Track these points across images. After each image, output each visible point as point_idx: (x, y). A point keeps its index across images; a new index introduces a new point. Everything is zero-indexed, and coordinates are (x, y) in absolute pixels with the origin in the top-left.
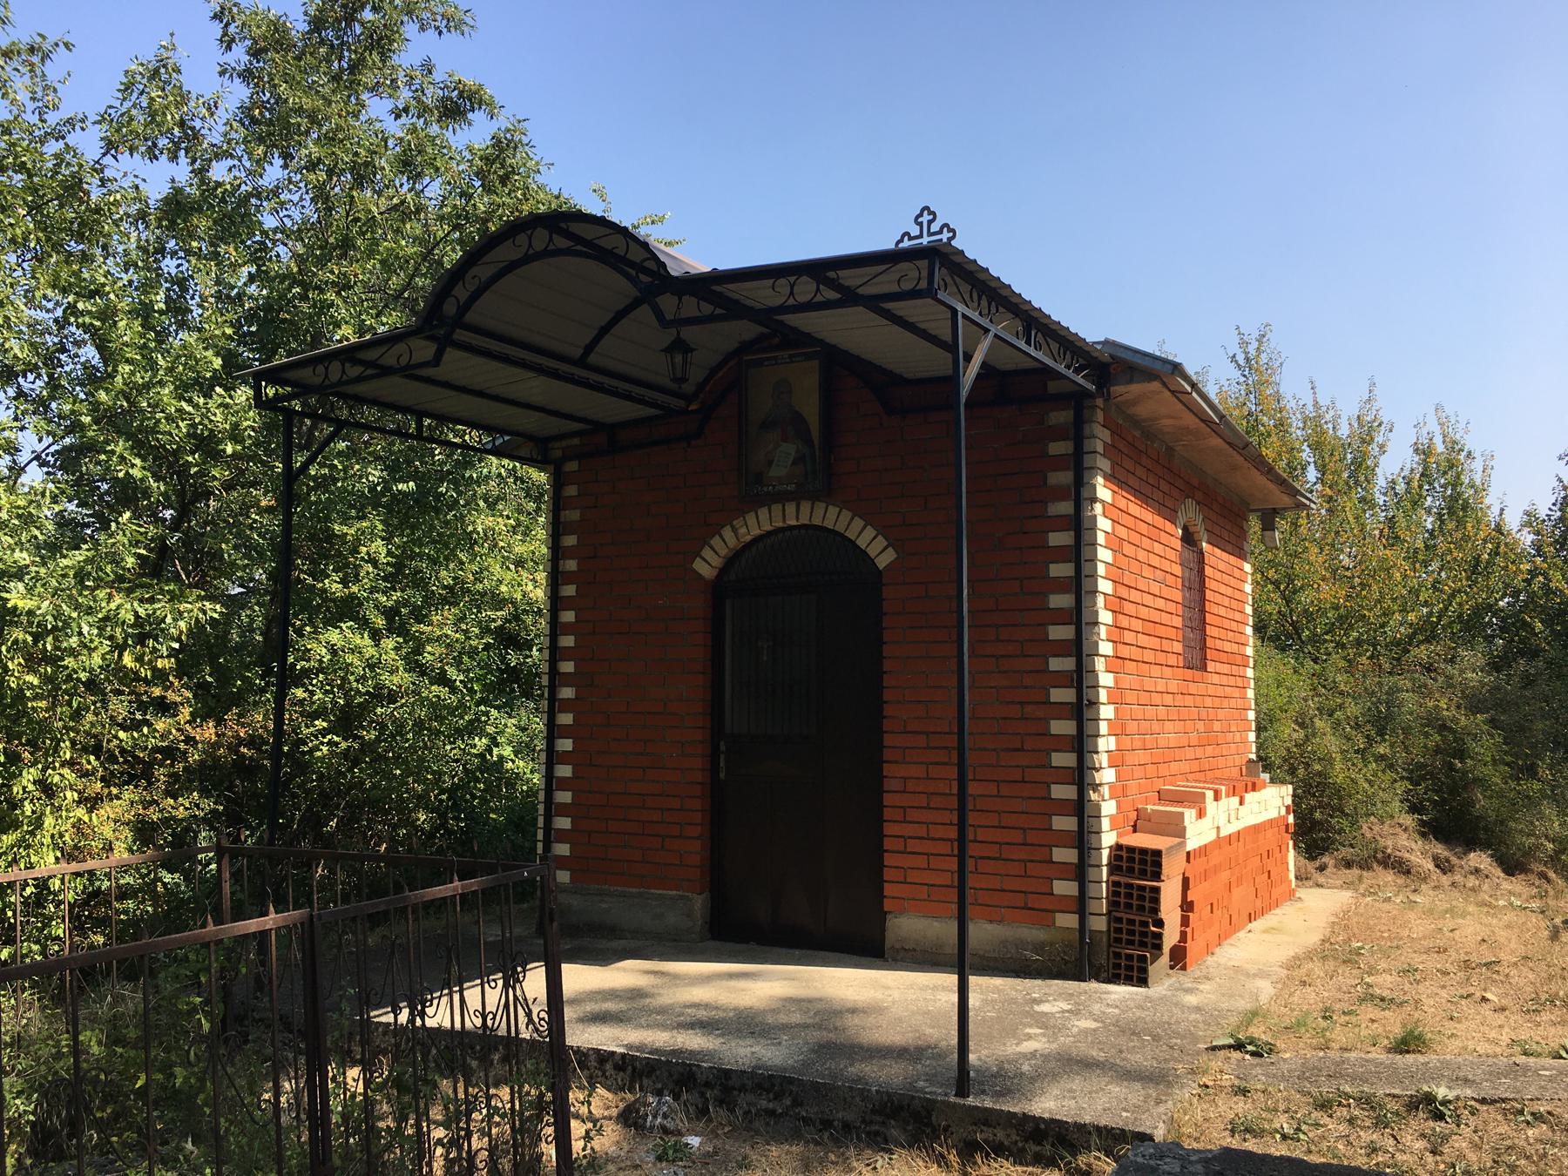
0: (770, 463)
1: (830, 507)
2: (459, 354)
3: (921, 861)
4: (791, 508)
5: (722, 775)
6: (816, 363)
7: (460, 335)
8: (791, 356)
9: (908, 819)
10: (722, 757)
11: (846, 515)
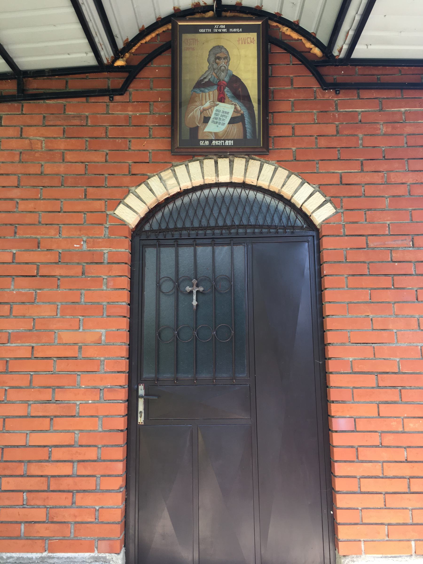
0: (206, 120)
1: (266, 166)
2: (155, 252)
3: (378, 500)
4: (224, 163)
5: (141, 420)
6: (254, 36)
7: (180, 242)
8: (227, 27)
9: (361, 458)
10: (141, 402)
11: (282, 173)
